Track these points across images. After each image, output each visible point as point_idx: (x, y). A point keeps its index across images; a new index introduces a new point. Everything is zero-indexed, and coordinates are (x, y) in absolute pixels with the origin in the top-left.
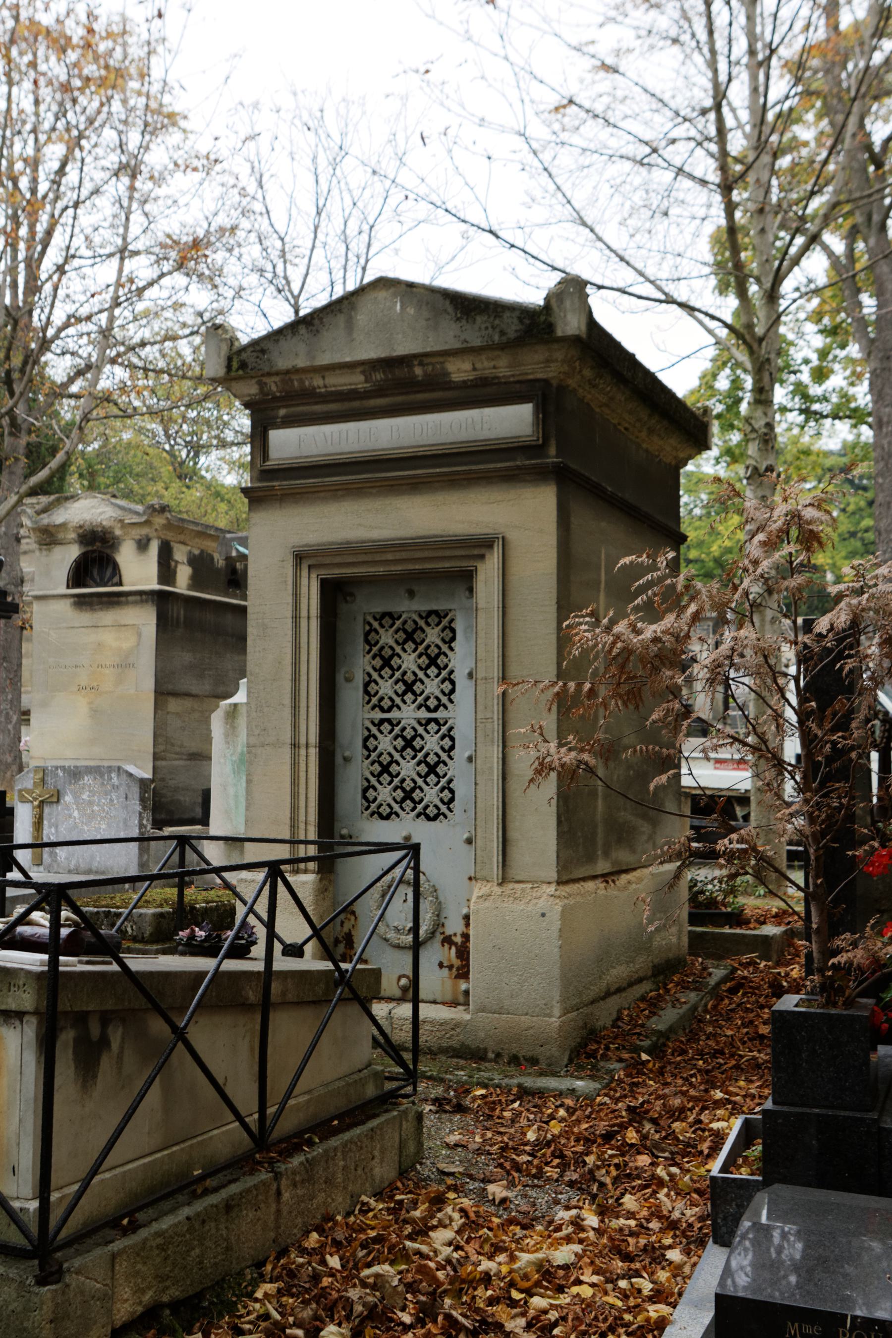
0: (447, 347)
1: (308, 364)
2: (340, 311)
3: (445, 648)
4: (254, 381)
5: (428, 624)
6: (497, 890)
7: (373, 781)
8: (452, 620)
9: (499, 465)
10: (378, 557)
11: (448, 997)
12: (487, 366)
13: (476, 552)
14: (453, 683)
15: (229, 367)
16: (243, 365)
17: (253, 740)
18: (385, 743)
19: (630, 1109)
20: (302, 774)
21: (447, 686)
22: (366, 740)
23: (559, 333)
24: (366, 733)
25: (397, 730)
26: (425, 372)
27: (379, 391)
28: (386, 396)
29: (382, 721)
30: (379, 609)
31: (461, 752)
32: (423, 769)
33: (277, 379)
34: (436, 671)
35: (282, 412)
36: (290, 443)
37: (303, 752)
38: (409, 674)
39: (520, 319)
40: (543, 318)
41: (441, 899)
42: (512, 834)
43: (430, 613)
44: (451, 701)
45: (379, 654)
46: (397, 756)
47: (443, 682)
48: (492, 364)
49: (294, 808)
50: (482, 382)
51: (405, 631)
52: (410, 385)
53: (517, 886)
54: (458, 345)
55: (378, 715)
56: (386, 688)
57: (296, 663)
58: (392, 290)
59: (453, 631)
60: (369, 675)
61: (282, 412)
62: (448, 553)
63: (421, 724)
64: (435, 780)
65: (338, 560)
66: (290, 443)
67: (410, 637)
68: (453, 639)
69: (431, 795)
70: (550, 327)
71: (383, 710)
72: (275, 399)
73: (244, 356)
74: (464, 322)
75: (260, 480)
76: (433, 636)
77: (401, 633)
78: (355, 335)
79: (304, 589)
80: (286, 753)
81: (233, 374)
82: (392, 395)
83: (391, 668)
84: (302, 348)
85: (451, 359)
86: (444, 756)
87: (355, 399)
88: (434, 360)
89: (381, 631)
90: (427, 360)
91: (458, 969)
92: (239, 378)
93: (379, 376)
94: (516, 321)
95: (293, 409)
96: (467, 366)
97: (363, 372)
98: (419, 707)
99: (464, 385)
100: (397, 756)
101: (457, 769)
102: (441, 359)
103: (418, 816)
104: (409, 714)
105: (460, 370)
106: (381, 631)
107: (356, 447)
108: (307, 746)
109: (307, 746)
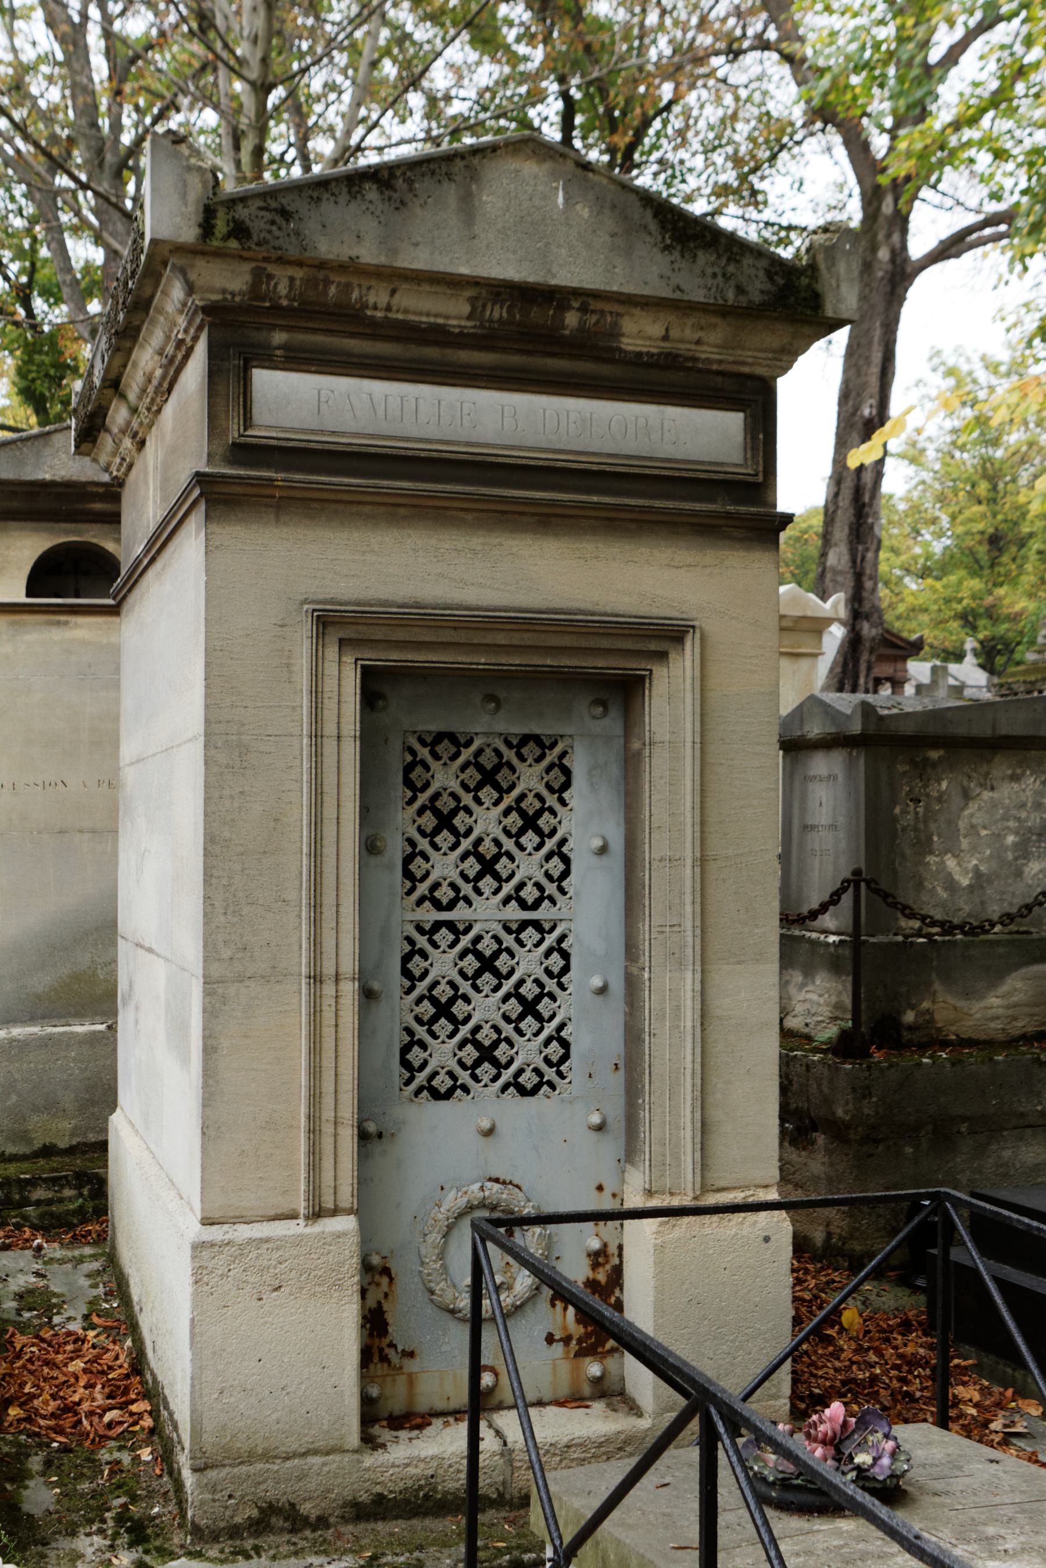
1: (383, 260)
2: (449, 176)
3: (551, 800)
4: (247, 267)
5: (522, 759)
7: (421, 1032)
8: (564, 754)
10: (477, 638)
11: (563, 1391)
13: (653, 646)
14: (566, 860)
15: (207, 227)
16: (239, 231)
18: (443, 964)
19: (85, 1387)
20: (328, 1032)
21: (556, 866)
22: (406, 959)
24: (408, 948)
25: (465, 941)
26: (582, 323)
27: (484, 339)
29: (437, 926)
31: (584, 978)
32: (514, 1007)
33: (299, 274)
35: (279, 337)
36: (292, 399)
37: (329, 989)
38: (487, 843)
39: (770, 275)
40: (804, 281)
42: (716, 1115)
43: (525, 739)
44: (563, 891)
45: (431, 806)
46: (465, 987)
47: (548, 857)
48: (696, 336)
50: (669, 361)
51: (480, 768)
52: (550, 341)
54: (665, 293)
55: (429, 915)
56: (444, 866)
57: (317, 823)
58: (548, 165)
59: (567, 772)
60: (411, 842)
62: (605, 643)
63: (508, 930)
64: (536, 1025)
65: (400, 635)
66: (292, 399)
67: (488, 778)
68: (567, 785)
69: (528, 1052)
71: (438, 906)
72: (276, 309)
73: (242, 213)
75: (232, 462)
76: (530, 778)
77: (471, 771)
78: (477, 229)
79: (330, 685)
80: (298, 997)
82: (504, 350)
83: (454, 831)
84: (369, 226)
85: (637, 312)
86: (551, 985)
87: (437, 343)
88: (607, 307)
89: (435, 765)
90: (595, 305)
91: (580, 1341)
92: (219, 254)
93: (497, 312)
94: (761, 273)
95: (301, 337)
96: (656, 330)
97: (472, 300)
98: (506, 901)
99: (637, 360)
100: (465, 987)
102: (620, 309)
105: (641, 333)
106: (435, 765)
107: (431, 431)
108: (337, 979)
109: (337, 979)
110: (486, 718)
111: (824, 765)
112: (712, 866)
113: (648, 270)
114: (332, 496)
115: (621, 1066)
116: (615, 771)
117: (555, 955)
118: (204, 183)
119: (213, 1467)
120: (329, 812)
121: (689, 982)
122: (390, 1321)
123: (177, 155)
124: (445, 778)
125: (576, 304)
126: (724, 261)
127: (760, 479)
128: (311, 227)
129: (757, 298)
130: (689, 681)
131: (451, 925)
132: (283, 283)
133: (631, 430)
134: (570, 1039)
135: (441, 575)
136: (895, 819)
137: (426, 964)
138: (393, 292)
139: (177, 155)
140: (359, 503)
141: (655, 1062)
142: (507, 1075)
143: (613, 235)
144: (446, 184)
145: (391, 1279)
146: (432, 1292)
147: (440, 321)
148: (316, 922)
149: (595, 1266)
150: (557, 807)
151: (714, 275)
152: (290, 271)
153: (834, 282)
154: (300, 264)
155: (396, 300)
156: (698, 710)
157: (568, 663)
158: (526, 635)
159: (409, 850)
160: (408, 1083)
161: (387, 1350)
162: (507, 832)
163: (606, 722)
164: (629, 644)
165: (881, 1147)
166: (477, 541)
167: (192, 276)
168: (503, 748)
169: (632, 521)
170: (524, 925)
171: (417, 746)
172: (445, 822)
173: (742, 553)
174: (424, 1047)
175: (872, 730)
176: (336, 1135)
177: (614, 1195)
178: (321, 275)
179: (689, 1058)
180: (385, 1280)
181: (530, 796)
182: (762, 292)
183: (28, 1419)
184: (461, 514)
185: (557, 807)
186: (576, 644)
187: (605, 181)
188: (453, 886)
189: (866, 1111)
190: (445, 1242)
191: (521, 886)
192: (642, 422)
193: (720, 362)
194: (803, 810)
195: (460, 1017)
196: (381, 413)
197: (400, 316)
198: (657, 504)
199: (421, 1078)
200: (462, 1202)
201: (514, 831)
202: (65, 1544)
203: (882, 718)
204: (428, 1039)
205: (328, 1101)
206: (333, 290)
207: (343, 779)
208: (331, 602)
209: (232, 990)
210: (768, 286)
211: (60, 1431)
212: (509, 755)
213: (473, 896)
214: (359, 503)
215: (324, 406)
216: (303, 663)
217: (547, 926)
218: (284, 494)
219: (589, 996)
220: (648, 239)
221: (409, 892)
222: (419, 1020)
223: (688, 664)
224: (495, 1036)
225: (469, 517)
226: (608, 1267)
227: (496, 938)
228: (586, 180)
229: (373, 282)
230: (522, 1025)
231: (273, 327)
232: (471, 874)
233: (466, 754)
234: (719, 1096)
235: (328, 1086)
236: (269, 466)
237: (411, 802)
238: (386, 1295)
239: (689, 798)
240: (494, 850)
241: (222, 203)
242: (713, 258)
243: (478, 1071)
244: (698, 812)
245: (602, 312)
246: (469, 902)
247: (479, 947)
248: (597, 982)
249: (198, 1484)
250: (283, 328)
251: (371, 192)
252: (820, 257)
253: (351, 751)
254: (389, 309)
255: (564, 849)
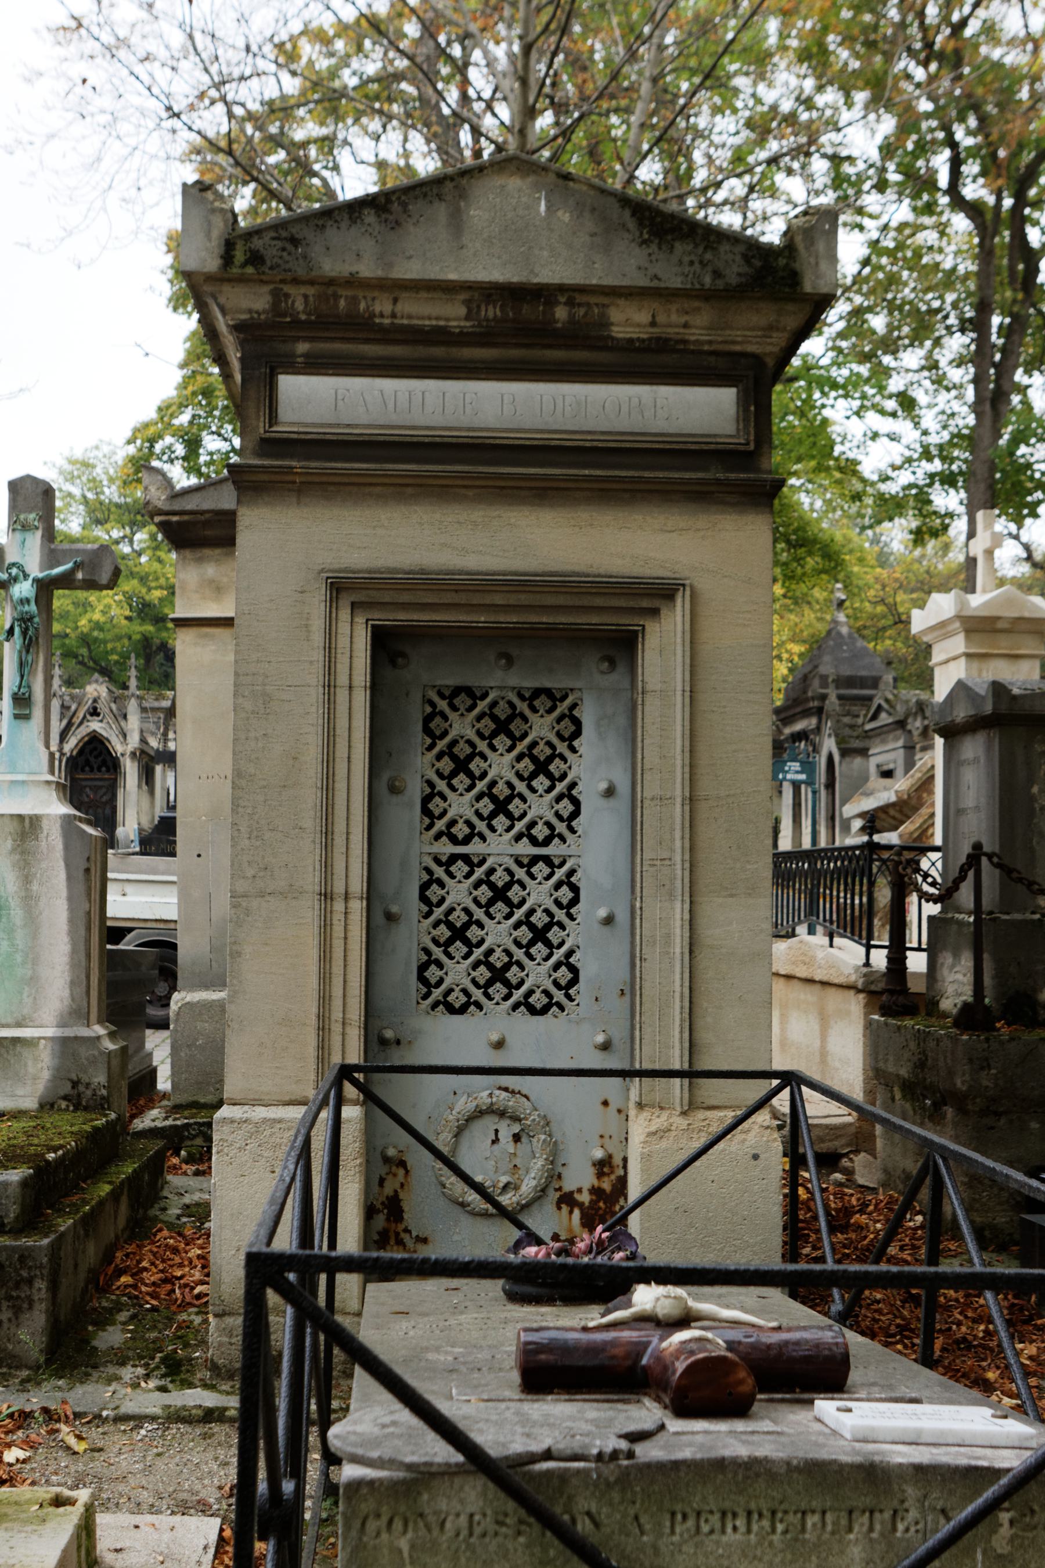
0: (626, 282)
1: (380, 273)
2: (440, 197)
3: (562, 748)
4: (266, 289)
5: (534, 710)
6: (681, 1122)
7: (438, 952)
8: (574, 706)
9: (687, 475)
10: (477, 599)
12: (673, 320)
13: (645, 603)
14: (576, 803)
15: (227, 258)
16: (255, 259)
17: (242, 886)
18: (459, 893)
21: (565, 807)
22: (424, 887)
23: (808, 288)
24: (426, 877)
25: (479, 872)
27: (483, 337)
28: (494, 345)
29: (453, 858)
30: (452, 681)
31: (591, 910)
33: (311, 291)
34: (547, 783)
35: (302, 347)
36: (311, 399)
37: (339, 906)
39: (747, 259)
40: (782, 262)
41: (557, 1136)
43: (537, 693)
45: (449, 752)
46: (479, 914)
48: (683, 319)
49: (324, 999)
50: (660, 345)
52: (544, 334)
53: (709, 1114)
54: (643, 282)
55: (446, 848)
56: (461, 805)
58: (531, 179)
59: (577, 723)
60: (431, 784)
61: (302, 347)
62: (599, 602)
63: (520, 864)
64: (545, 951)
65: (405, 598)
66: (311, 399)
67: (502, 727)
68: (577, 733)
69: (537, 974)
70: (794, 278)
71: (454, 840)
72: (296, 323)
73: (257, 243)
74: (654, 247)
76: (541, 727)
77: (486, 721)
79: (343, 642)
80: (309, 911)
81: (235, 270)
82: (505, 345)
84: (368, 246)
85: (621, 302)
86: (560, 915)
88: (593, 300)
89: (453, 716)
90: (580, 298)
92: (242, 280)
93: (492, 312)
94: (738, 258)
96: (643, 317)
97: (467, 303)
98: (518, 838)
99: (629, 346)
100: (479, 914)
101: (581, 934)
102: (605, 300)
103: (515, 1007)
104: (500, 848)
105: (629, 322)
106: (453, 716)
107: (437, 420)
108: (347, 898)
109: (347, 898)
110: (499, 674)
111: (973, 747)
112: (702, 807)
113: (626, 264)
114: (346, 480)
115: (627, 991)
116: (622, 721)
117: (565, 888)
118: (226, 221)
119: (230, 1314)
120: (341, 751)
121: (678, 911)
122: (406, 1208)
123: (204, 201)
124: (462, 727)
125: (562, 299)
126: (700, 250)
127: (752, 447)
128: (316, 251)
129: (733, 280)
130: (679, 635)
131: (466, 858)
132: (298, 300)
133: (625, 409)
134: (578, 965)
135: (444, 545)
136: (1032, 799)
137: (443, 892)
138: (395, 301)
139: (204, 201)
140: (371, 484)
141: (646, 985)
142: (518, 995)
143: (593, 235)
144: (436, 204)
145: (407, 1172)
146: (444, 1186)
147: (442, 323)
148: (327, 846)
149: (600, 1175)
150: (567, 754)
151: (692, 263)
152: (303, 290)
153: (812, 260)
154: (312, 283)
155: (399, 307)
156: (688, 661)
157: (563, 620)
158: (523, 597)
159: (428, 790)
160: (425, 997)
161: (403, 1235)
162: (519, 776)
163: (614, 677)
164: (622, 603)
165: (1003, 1121)
166: (477, 514)
167: (222, 300)
168: (516, 700)
169: (625, 491)
170: (535, 860)
171: (436, 699)
172: (461, 766)
173: (734, 517)
174: (440, 965)
175: (1004, 709)
176: (344, 1034)
177: (619, 1111)
178: (330, 291)
179: (678, 983)
180: (401, 1172)
181: (542, 744)
182: (739, 275)
183: (135, 1287)
184: (463, 491)
185: (567, 754)
186: (570, 603)
187: (585, 188)
188: (468, 823)
189: (985, 1083)
190: (457, 1143)
191: (533, 824)
192: (635, 401)
193: (710, 342)
194: (957, 797)
195: (474, 941)
196: (391, 406)
197: (405, 322)
198: (647, 474)
199: (437, 993)
200: (471, 1106)
201: (526, 775)
202: (111, 1370)
203: (1015, 698)
204: (444, 959)
205: (337, 1003)
206: (342, 303)
207: (354, 724)
208: (340, 571)
209: (255, 903)
210: (745, 269)
211: (154, 1296)
212: (522, 707)
213: (487, 832)
214: (371, 484)
215: (340, 403)
216: (318, 624)
217: (556, 862)
218: (303, 479)
219: (596, 926)
220: (626, 235)
221: (429, 828)
222: (435, 941)
223: (679, 619)
224: (506, 959)
225: (470, 493)
226: (613, 1177)
227: (508, 871)
228: (567, 188)
229: (376, 294)
230: (533, 951)
231: (297, 339)
232: (485, 813)
233: (482, 706)
234: (709, 1020)
235: (337, 991)
236: (292, 457)
237: (430, 748)
238: (402, 1185)
239: (679, 742)
240: (507, 792)
241: (240, 236)
242: (691, 247)
243: (490, 991)
244: (687, 755)
245: (588, 305)
246: (483, 839)
247: (492, 878)
248: (602, 913)
249: (217, 1328)
250: (306, 339)
251: (370, 217)
252: (798, 239)
253: (361, 700)
254: (394, 315)
255: (574, 792)
